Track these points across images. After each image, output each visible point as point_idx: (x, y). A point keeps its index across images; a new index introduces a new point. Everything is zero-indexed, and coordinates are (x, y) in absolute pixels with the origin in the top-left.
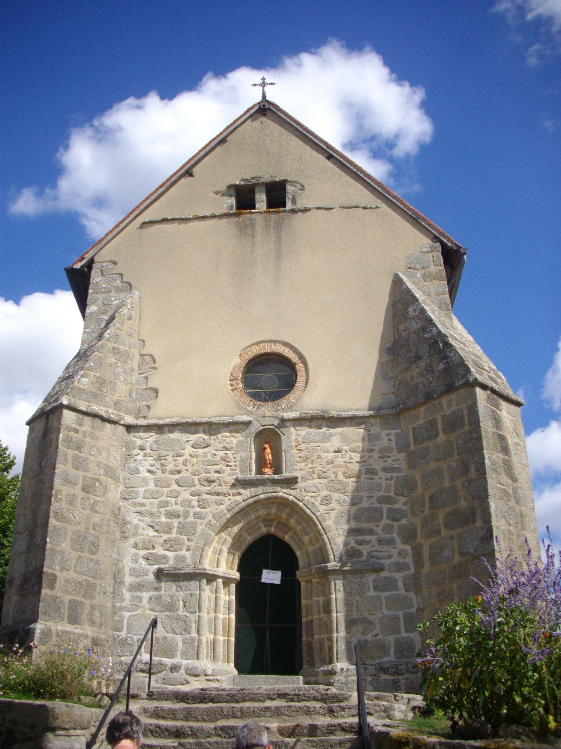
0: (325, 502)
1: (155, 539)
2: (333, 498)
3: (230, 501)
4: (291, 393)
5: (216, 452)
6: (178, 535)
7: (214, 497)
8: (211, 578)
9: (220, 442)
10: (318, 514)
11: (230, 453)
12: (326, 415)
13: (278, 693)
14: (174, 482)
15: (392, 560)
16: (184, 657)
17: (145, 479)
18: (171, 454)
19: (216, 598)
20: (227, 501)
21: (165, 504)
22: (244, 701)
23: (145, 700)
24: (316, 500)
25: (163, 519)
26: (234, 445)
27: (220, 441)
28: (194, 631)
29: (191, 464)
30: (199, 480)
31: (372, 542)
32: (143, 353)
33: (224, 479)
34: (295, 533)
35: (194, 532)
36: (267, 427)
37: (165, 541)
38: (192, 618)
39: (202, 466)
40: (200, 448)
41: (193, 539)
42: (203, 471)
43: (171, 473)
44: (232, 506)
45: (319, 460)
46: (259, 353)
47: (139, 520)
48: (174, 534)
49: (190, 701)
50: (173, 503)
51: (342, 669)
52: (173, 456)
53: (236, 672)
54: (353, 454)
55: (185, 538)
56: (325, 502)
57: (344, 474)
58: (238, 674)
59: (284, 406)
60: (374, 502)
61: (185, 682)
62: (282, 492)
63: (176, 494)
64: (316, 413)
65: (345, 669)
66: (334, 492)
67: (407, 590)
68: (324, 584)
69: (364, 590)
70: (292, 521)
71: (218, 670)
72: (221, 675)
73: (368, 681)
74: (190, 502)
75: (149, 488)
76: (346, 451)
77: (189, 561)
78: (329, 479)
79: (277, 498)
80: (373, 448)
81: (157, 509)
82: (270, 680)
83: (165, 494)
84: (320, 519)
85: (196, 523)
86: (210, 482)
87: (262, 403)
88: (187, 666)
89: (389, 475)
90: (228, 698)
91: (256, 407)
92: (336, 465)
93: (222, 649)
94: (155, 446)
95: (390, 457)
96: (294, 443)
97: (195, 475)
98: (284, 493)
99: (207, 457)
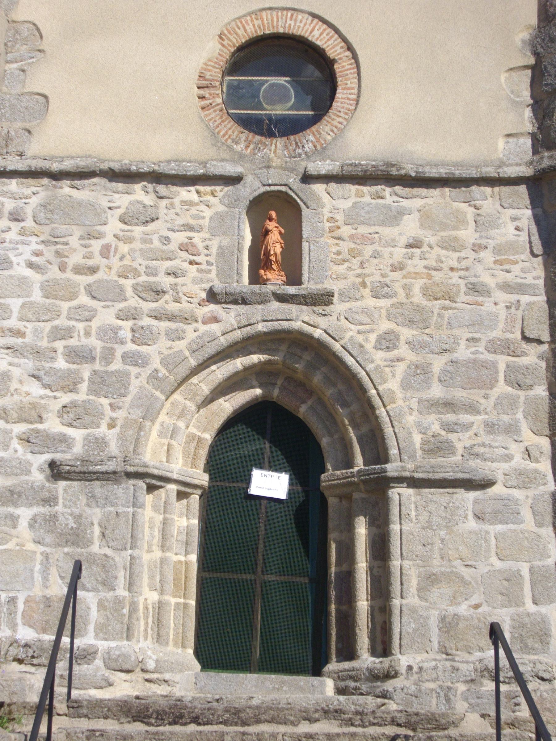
0: (385, 345)
1: (43, 402)
2: (401, 337)
3: (196, 334)
4: (324, 121)
5: (170, 234)
6: (91, 397)
7: (164, 325)
8: (154, 482)
9: (177, 214)
10: (370, 367)
11: (197, 238)
12: (394, 172)
13: (322, 709)
14: (83, 290)
15: (513, 463)
16: (101, 635)
17: (23, 281)
18: (77, 232)
19: (165, 522)
20: (191, 333)
21: (63, 333)
22: (258, 721)
23: (64, 717)
24: (367, 340)
25: (61, 364)
26: (206, 222)
27: (178, 210)
28: (122, 586)
29: (118, 256)
30: (135, 288)
31: (474, 427)
32: (15, 19)
33: (185, 289)
34: (320, 401)
35: (122, 391)
36: (296, 197)
37: (65, 407)
38: (117, 559)
39: (140, 260)
40: (137, 224)
41: (121, 404)
42: (142, 269)
43: (78, 270)
44: (201, 342)
45: (375, 261)
46: (260, 33)
47: (10, 364)
48: (82, 395)
49: (153, 721)
50: (82, 333)
51: (410, 668)
52: (82, 238)
53: (198, 666)
54: (443, 252)
55: (105, 402)
56: (385, 345)
57: (425, 291)
58: (201, 671)
59: (309, 147)
60: (481, 349)
61: (104, 683)
62: (301, 319)
63: (87, 314)
64: (373, 166)
65: (415, 669)
66: (403, 326)
67: (539, 525)
68: (377, 503)
69: (457, 518)
70: (317, 379)
71: (167, 661)
72: (172, 671)
73: (459, 692)
74: (116, 330)
75: (32, 299)
76: (431, 247)
77: (114, 448)
78: (395, 300)
79: (288, 332)
80: (484, 242)
81: (49, 342)
82: (267, 684)
83: (64, 313)
84: (372, 376)
85: (127, 374)
86: (159, 292)
87: (263, 139)
88: (108, 653)
89: (513, 298)
90: (227, 715)
91: (252, 146)
92: (409, 273)
93: (172, 622)
94: (42, 215)
95: (517, 262)
96: (328, 225)
97: (126, 278)
98: (304, 322)
99: (151, 242)
